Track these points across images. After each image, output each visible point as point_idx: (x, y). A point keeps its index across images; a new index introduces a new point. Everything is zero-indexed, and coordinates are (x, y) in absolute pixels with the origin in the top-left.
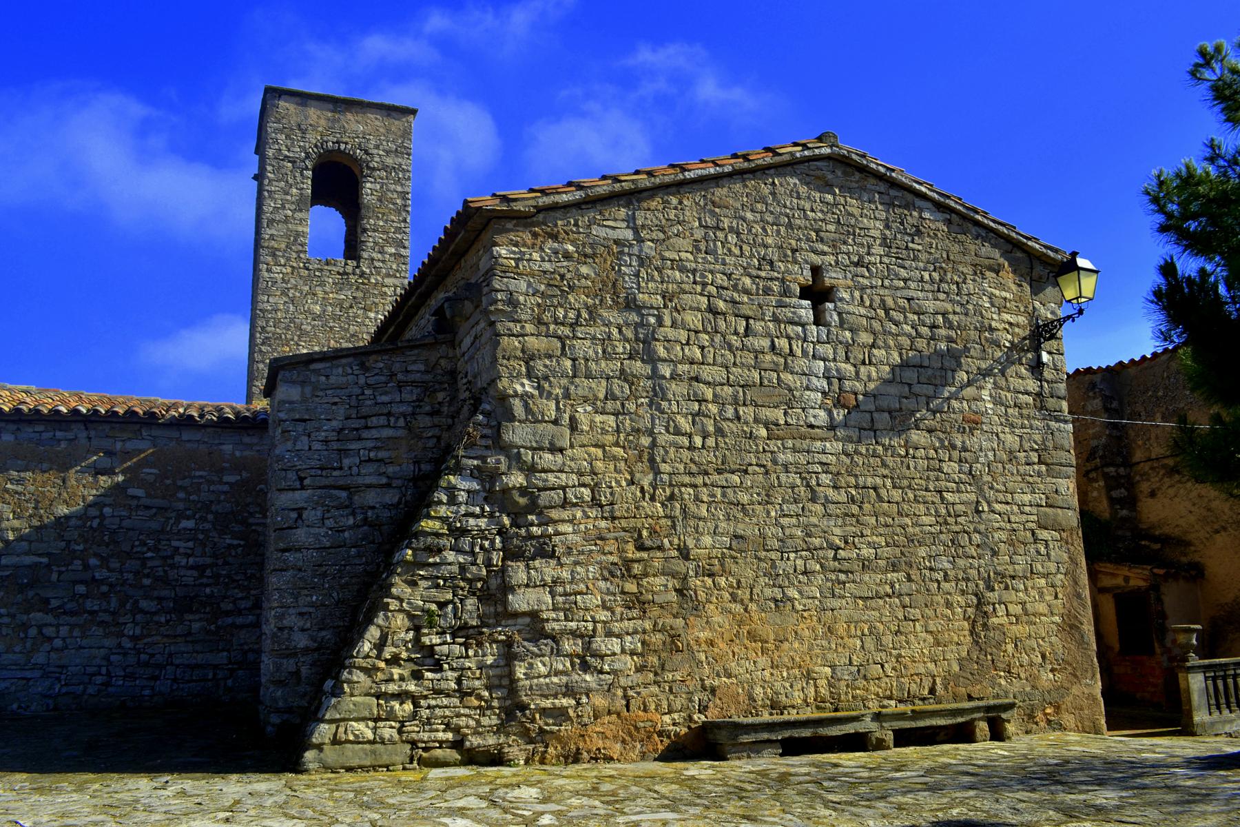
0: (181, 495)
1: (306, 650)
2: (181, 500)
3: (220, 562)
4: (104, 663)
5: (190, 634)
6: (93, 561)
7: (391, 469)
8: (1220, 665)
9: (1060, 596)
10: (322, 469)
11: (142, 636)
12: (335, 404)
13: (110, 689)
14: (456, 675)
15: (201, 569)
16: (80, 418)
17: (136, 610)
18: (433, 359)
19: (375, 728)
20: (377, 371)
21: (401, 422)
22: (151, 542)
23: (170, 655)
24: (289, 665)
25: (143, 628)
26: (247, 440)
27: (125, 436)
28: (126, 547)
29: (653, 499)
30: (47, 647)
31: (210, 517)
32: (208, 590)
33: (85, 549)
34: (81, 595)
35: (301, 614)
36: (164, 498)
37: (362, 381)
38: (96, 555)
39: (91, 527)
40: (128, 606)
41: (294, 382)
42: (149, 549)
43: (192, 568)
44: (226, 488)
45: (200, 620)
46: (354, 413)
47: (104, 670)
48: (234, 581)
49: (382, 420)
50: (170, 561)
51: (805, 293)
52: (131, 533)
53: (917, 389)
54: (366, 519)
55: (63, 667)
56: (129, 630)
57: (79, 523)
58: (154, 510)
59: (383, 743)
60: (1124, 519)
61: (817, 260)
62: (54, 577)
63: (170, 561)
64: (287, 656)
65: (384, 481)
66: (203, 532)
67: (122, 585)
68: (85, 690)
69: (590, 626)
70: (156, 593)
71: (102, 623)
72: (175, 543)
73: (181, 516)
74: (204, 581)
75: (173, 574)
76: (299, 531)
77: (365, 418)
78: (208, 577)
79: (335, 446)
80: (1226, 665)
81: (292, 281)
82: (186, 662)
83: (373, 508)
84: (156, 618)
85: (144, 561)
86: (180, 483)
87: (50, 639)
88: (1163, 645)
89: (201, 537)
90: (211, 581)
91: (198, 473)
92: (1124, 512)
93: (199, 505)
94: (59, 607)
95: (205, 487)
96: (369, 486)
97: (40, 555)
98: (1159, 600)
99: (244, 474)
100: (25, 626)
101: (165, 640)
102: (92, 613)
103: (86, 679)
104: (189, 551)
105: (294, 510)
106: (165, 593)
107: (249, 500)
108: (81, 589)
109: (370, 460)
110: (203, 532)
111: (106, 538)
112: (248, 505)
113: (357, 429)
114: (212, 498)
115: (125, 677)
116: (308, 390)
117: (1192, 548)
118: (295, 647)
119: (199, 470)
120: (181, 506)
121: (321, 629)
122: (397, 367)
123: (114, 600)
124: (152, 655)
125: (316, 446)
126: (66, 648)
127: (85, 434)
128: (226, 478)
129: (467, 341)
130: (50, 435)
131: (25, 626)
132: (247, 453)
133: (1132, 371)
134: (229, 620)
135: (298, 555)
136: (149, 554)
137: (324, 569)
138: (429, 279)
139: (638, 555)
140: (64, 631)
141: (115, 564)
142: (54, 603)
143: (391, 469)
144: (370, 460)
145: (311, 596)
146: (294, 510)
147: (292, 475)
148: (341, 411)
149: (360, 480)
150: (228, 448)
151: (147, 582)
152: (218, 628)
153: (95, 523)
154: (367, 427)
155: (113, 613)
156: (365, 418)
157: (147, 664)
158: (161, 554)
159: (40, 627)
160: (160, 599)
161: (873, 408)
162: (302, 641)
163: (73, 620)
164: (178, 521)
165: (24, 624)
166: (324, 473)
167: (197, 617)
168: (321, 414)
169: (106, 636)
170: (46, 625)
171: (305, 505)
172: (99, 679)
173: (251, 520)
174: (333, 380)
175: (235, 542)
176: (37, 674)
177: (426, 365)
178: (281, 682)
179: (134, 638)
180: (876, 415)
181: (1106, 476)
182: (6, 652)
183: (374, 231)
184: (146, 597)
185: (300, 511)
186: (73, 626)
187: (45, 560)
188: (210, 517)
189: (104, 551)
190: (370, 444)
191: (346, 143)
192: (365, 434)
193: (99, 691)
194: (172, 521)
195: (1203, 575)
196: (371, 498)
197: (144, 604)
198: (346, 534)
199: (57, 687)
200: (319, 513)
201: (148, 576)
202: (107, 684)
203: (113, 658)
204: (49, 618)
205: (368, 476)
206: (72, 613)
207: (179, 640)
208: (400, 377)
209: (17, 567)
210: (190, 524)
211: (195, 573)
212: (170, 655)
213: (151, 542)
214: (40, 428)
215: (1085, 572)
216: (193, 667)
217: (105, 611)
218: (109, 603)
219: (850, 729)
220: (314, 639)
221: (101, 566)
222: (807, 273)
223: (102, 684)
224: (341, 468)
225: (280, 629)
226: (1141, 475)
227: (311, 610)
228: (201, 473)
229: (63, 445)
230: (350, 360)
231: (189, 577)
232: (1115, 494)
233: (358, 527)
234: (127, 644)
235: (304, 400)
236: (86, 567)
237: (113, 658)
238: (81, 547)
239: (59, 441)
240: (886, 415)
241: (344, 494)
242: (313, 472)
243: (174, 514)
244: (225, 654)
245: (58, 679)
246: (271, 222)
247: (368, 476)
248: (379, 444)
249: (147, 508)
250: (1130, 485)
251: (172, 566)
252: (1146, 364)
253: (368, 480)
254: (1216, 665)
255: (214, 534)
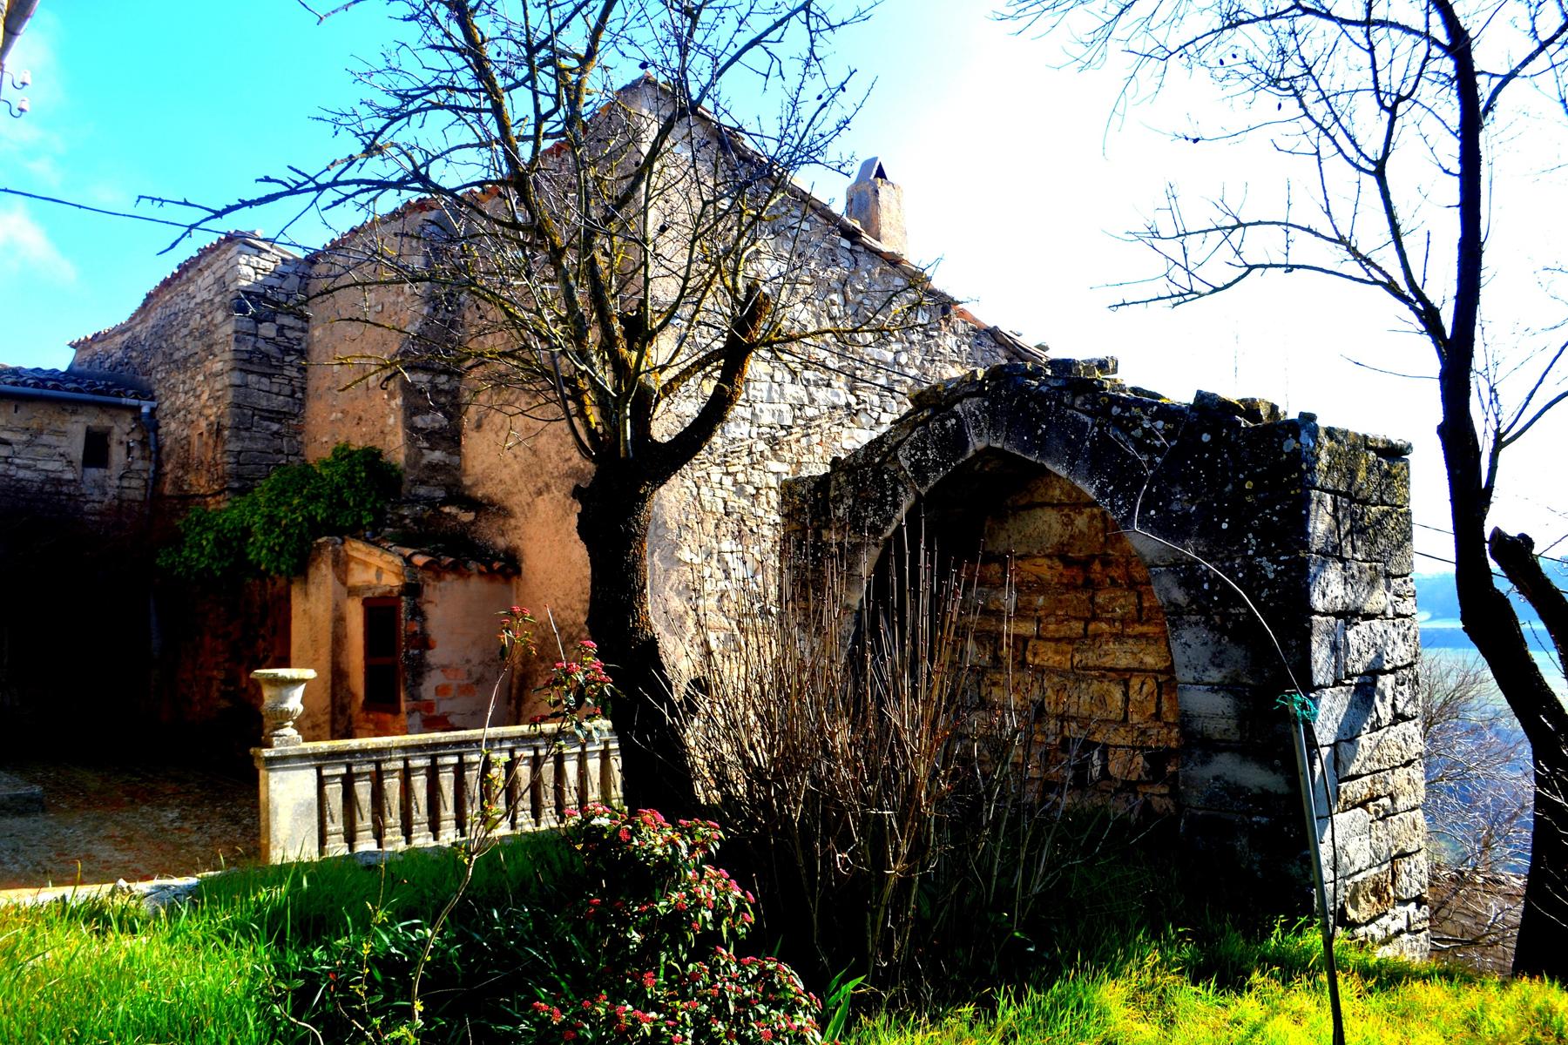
8: (364, 752)
60: (434, 467)
80: (379, 751)
88: (414, 696)
92: (437, 456)
98: (417, 613)
117: (513, 522)
181: (407, 388)
195: (518, 571)
215: (1494, 683)
232: (419, 421)
250: (454, 408)
254: (351, 753)
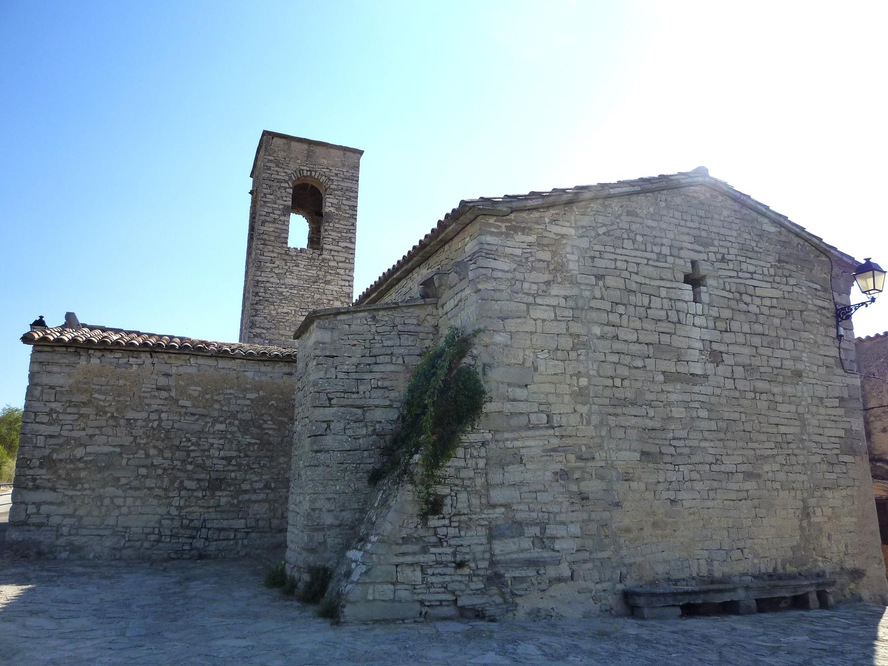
0: (217, 406)
1: (331, 526)
2: (216, 410)
3: (242, 455)
4: (157, 525)
5: (219, 506)
6: (153, 452)
7: (392, 395)
9: (856, 503)
10: (345, 392)
11: (186, 507)
12: (354, 345)
13: (161, 545)
14: (452, 550)
15: (229, 459)
16: (147, 349)
17: (182, 487)
18: (423, 316)
19: (395, 591)
20: (384, 323)
21: (400, 361)
22: (194, 440)
23: (204, 521)
24: (319, 537)
25: (186, 500)
26: (263, 369)
27: (179, 362)
28: (176, 442)
29: (589, 423)
30: (116, 512)
31: (236, 422)
32: (233, 475)
33: (147, 443)
34: (143, 476)
35: (329, 499)
36: (205, 407)
37: (373, 329)
38: (154, 447)
39: (152, 427)
40: (176, 485)
41: (326, 328)
42: (193, 444)
43: (223, 458)
44: (248, 402)
45: (227, 496)
46: (367, 352)
47: (156, 531)
48: (251, 469)
49: (387, 359)
50: (207, 453)
51: (688, 279)
52: (180, 432)
53: (761, 350)
54: (375, 430)
55: (127, 528)
56: (176, 502)
57: (144, 423)
58: (197, 417)
59: (400, 601)
61: (696, 256)
62: (124, 462)
63: (207, 453)
64: (318, 530)
65: (388, 403)
66: (231, 433)
67: (172, 469)
68: (142, 545)
69: (546, 516)
70: (196, 476)
71: (157, 496)
72: (211, 441)
73: (216, 421)
74: (231, 468)
75: (208, 462)
76: (327, 438)
77: (375, 356)
78: (234, 465)
79: (354, 376)
81: (277, 262)
82: (216, 526)
83: (380, 422)
84: (195, 494)
85: (188, 452)
86: (216, 398)
87: (119, 507)
89: (229, 436)
90: (235, 468)
91: (228, 391)
93: (229, 414)
94: (127, 484)
95: (233, 401)
96: (377, 407)
97: (115, 446)
99: (261, 393)
100: (101, 497)
101: (201, 510)
102: (150, 489)
103: (143, 536)
104: (221, 447)
105: (324, 422)
106: (202, 476)
107: (264, 411)
108: (143, 471)
109: (378, 388)
110: (231, 433)
111: (162, 435)
112: (263, 415)
113: (369, 365)
114: (238, 409)
115: (171, 536)
116: (336, 334)
118: (324, 524)
119: (230, 389)
120: (216, 414)
121: (342, 511)
122: (398, 321)
123: (166, 480)
124: (192, 520)
125: (341, 375)
126: (130, 513)
127: (150, 360)
128: (248, 396)
129: (451, 304)
130: (125, 360)
131: (101, 497)
132: (263, 378)
133: (867, 344)
134: (247, 497)
135: (327, 455)
136: (192, 448)
137: (345, 466)
138: (415, 259)
139: (578, 464)
140: (129, 501)
141: (168, 454)
142: (123, 481)
143: (392, 395)
144: (378, 388)
145: (336, 486)
146: (324, 422)
147: (323, 397)
148: (359, 351)
149: (371, 402)
150: (250, 374)
151: (190, 467)
152: (239, 502)
153: (155, 424)
154: (376, 363)
155: (165, 490)
156: (375, 356)
157: (188, 527)
158: (201, 448)
159: (112, 498)
160: (199, 480)
161: (733, 363)
162: (329, 519)
163: (137, 493)
164: (213, 425)
165: (100, 496)
166: (346, 395)
167: (225, 493)
168: (345, 352)
169: (159, 506)
170: (117, 497)
171: (332, 419)
172: (153, 537)
173: (265, 426)
174: (353, 327)
175: (253, 441)
176: (108, 532)
177: (418, 320)
178: (312, 549)
179: (179, 508)
180: (734, 368)
182: (87, 516)
183: (332, 230)
184: (189, 479)
185: (328, 423)
186: (136, 498)
187: (118, 450)
188: (236, 422)
189: (160, 445)
190: (378, 376)
191: (316, 172)
192: (375, 368)
193: (153, 546)
194: (209, 425)
196: (378, 415)
197: (187, 484)
198: (361, 441)
199: (122, 542)
200: (342, 425)
201: (191, 463)
202: (158, 541)
203: (163, 522)
204: (120, 492)
205: (377, 398)
206: (136, 489)
207: (211, 510)
208: (400, 328)
209: (97, 454)
210: (222, 427)
211: (224, 462)
212: (204, 521)
213: (194, 440)
214: (118, 355)
216: (220, 530)
217: (159, 488)
218: (162, 482)
219: (727, 597)
220: (337, 518)
221: (158, 455)
222: (689, 265)
223: (155, 541)
224: (358, 393)
225: (313, 510)
226: (875, 417)
227: (335, 496)
228: (231, 391)
229: (135, 368)
230: (366, 314)
231: (220, 465)
233: (370, 436)
234: (174, 512)
235: (333, 341)
236: (147, 456)
237: (163, 522)
238: (144, 441)
239: (131, 365)
240: (741, 368)
241: (360, 411)
242: (338, 395)
243: (210, 420)
244: (243, 521)
245: (124, 536)
246: (264, 223)
247: (377, 398)
248: (385, 376)
249: (193, 414)
251: (208, 457)
252: (878, 340)
253: (377, 402)
255: (238, 435)
